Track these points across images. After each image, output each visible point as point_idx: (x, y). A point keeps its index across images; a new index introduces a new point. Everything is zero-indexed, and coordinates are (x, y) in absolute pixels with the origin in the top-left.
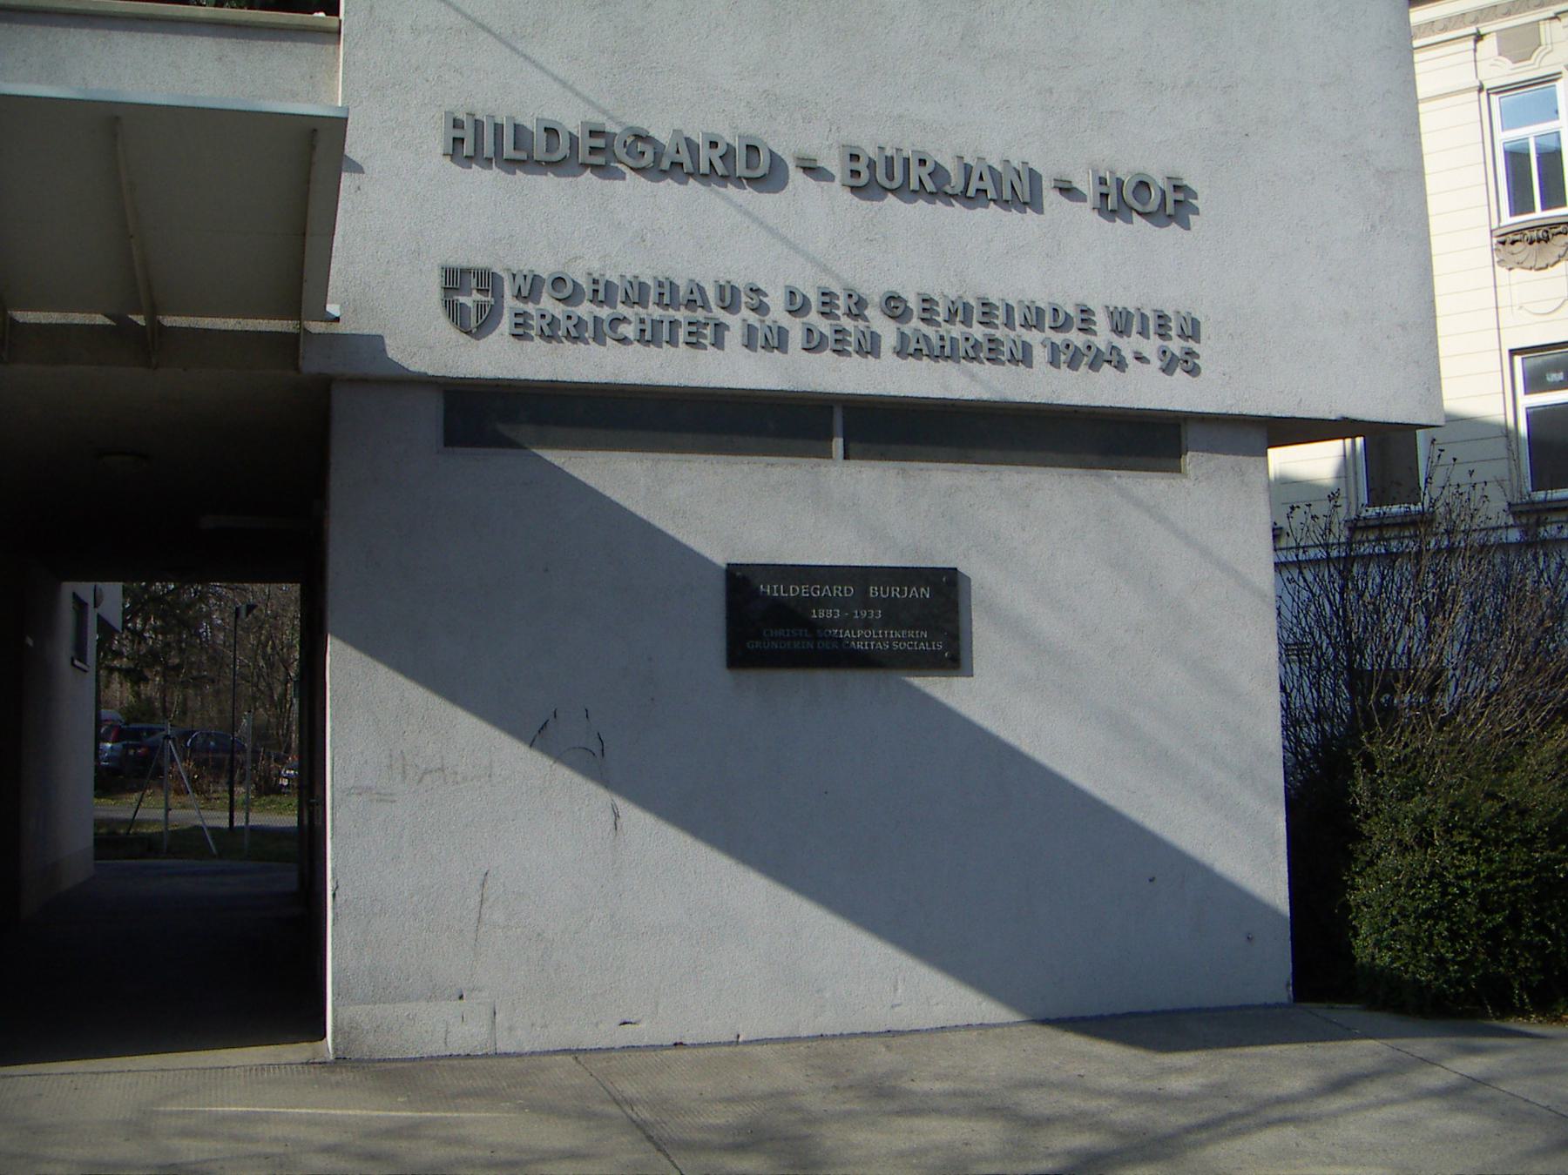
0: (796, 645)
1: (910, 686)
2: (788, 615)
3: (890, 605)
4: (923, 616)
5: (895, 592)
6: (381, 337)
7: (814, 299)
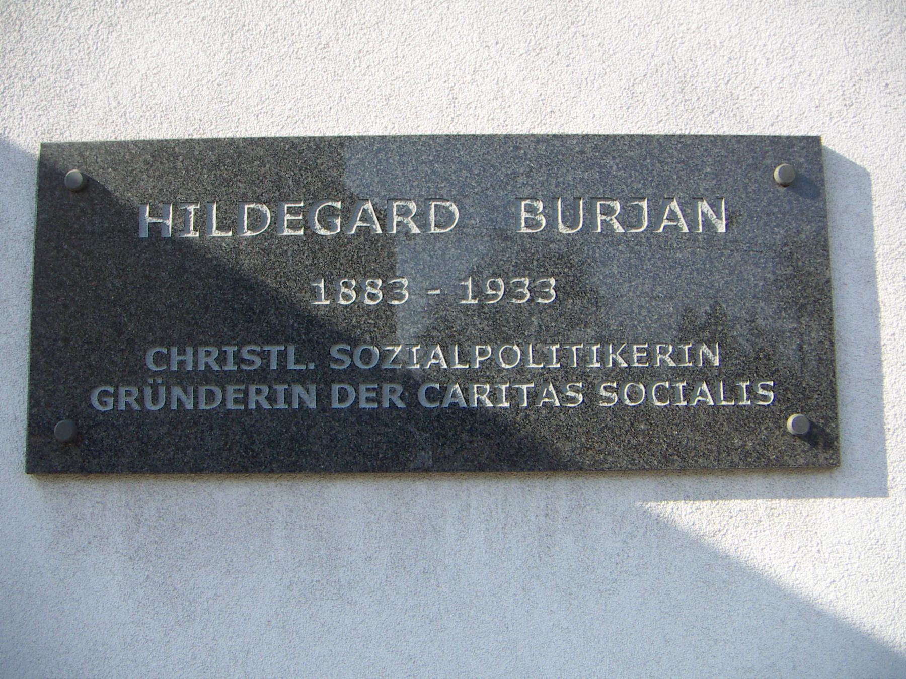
0: (257, 398)
1: (664, 528)
2: (241, 302)
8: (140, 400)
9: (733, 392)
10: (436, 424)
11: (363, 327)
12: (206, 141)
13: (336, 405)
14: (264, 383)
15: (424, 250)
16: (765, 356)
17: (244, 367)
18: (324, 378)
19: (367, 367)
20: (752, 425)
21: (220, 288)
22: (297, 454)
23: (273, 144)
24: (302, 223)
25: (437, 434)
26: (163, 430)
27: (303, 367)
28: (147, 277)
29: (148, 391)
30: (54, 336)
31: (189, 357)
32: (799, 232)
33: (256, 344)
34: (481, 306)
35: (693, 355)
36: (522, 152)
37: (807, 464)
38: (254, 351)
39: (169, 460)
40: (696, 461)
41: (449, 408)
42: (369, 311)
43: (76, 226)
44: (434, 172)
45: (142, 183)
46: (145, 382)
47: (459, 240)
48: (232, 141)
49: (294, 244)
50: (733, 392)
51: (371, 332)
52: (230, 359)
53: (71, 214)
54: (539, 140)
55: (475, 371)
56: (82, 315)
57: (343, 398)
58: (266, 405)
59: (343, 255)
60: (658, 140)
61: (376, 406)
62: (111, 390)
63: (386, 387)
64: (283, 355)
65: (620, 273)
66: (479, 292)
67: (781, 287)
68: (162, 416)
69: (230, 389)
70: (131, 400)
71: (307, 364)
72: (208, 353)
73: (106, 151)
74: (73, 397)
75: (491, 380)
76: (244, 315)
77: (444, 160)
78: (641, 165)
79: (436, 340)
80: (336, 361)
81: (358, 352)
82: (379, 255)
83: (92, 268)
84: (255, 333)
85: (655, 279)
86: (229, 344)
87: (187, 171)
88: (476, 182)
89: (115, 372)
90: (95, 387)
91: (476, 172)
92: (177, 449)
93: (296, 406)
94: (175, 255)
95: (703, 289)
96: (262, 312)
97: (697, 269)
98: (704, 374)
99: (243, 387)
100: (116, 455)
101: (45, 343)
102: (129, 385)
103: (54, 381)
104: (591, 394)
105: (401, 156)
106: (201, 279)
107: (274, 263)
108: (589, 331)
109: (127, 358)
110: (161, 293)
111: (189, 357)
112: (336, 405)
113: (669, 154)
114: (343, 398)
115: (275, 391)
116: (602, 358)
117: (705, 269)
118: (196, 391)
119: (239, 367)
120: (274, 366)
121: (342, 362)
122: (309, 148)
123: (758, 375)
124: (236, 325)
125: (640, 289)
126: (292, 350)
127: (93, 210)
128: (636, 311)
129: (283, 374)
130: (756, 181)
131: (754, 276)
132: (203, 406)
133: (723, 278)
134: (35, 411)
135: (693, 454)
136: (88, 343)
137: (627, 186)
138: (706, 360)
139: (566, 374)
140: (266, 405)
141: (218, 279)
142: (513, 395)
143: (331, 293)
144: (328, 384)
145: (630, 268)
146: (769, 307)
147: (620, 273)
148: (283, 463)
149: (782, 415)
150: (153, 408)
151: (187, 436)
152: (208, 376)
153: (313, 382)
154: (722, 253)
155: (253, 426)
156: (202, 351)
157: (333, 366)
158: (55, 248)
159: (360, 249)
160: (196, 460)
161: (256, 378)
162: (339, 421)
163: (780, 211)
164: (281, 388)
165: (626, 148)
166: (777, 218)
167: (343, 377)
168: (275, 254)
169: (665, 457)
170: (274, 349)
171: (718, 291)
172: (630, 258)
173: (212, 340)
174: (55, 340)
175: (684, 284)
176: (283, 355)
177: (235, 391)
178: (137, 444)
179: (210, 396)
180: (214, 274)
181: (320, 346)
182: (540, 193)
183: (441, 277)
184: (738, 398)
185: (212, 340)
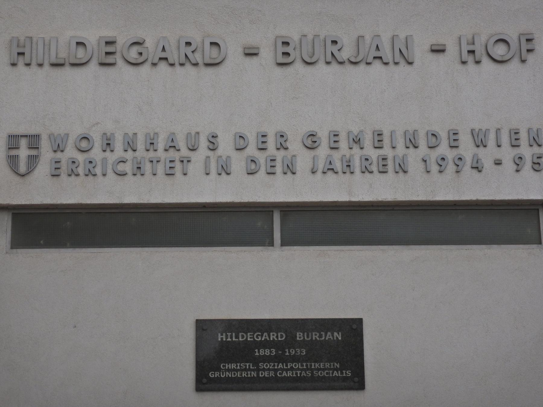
3: (310, 345)
4: (335, 351)
5: (315, 336)
7: (443, 135)
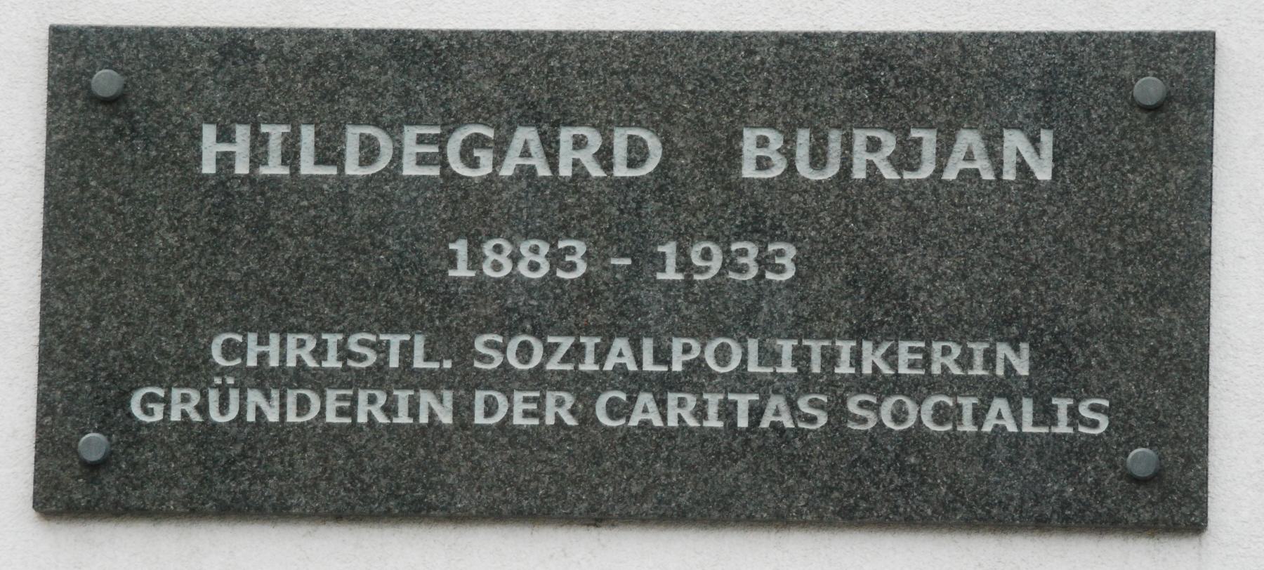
0: (369, 409)
2: (371, 261)
5: (870, 154)
6: (1214, 34)
8: (203, 409)
9: (1046, 414)
10: (620, 449)
11: (522, 309)
12: (300, 32)
13: (479, 419)
14: (380, 388)
15: (611, 202)
16: (1099, 364)
17: (351, 363)
18: (465, 381)
19: (526, 367)
20: (1074, 462)
21: (321, 250)
22: (424, 486)
23: (398, 40)
24: (439, 158)
25: (621, 463)
26: (236, 450)
27: (435, 365)
28: (214, 231)
29: (213, 395)
30: (77, 313)
31: (273, 348)
32: (1165, 180)
33: (370, 331)
34: (689, 282)
35: (990, 358)
36: (758, 58)
37: (1155, 522)
38: (367, 341)
39: (243, 492)
40: (989, 512)
41: (639, 427)
42: (526, 283)
43: (108, 153)
44: (628, 87)
45: (206, 92)
46: (209, 383)
47: (662, 189)
48: (337, 35)
49: (427, 189)
50: (1046, 414)
51: (533, 318)
52: (332, 352)
53: (100, 135)
54: (782, 40)
55: (677, 375)
56: (119, 285)
57: (490, 410)
58: (381, 419)
59: (496, 206)
60: (960, 40)
61: (536, 422)
62: (160, 392)
63: (551, 397)
64: (407, 349)
65: (892, 239)
66: (685, 265)
67: (1131, 261)
68: (235, 429)
69: (331, 395)
70: (189, 408)
71: (441, 362)
72: (301, 344)
73: (153, 43)
74: (105, 402)
75: (698, 390)
76: (354, 290)
77: (644, 69)
78: (932, 78)
79: (624, 330)
80: (482, 358)
81: (513, 345)
82: (547, 207)
83: (133, 215)
84: (368, 315)
85: (941, 248)
86: (330, 331)
87: (273, 76)
88: (689, 103)
89: (167, 367)
90: (137, 388)
91: (690, 88)
92: (255, 477)
93: (424, 419)
94: (254, 200)
95: (1013, 263)
96: (379, 286)
97: (1005, 235)
98: (1008, 388)
99: (350, 392)
100: (166, 484)
101: (64, 324)
102: (187, 386)
103: (76, 379)
104: (837, 412)
105: (582, 62)
106: (291, 235)
107: (397, 216)
108: (841, 321)
109: (185, 347)
110: (234, 255)
111: (273, 348)
112: (479, 419)
113: (974, 61)
114: (490, 410)
115: (395, 400)
116: (857, 359)
117: (1017, 235)
118: (283, 397)
119: (345, 364)
120: (394, 362)
121: (491, 359)
122: (450, 47)
123: (1086, 391)
124: (341, 304)
125: (919, 262)
126: (419, 342)
127: (133, 130)
128: (911, 294)
129: (408, 377)
130: (1106, 103)
131: (1092, 245)
132: (292, 417)
133: (1043, 248)
134: (48, 420)
135: (983, 502)
136: (128, 325)
137: (909, 111)
138: (1009, 368)
139: (805, 381)
140: (381, 419)
141: (317, 237)
142: (728, 411)
143: (475, 260)
144: (471, 391)
145: (906, 232)
146: (1110, 292)
147: (892, 239)
148: (404, 499)
149: (1121, 450)
150: (814, 176)
151: (270, 459)
152: (300, 376)
153: (449, 388)
154: (1044, 212)
155: (364, 447)
156: (292, 339)
157: (477, 365)
158: (77, 185)
159: (520, 198)
160: (281, 494)
161: (370, 380)
162: (483, 443)
163: (1138, 147)
164: (403, 396)
165: (910, 53)
166: (1132, 158)
167: (492, 380)
168: (399, 202)
169: (943, 504)
170: (395, 340)
171: (1034, 267)
172: (907, 217)
173: (308, 324)
174: (78, 319)
175: (984, 256)
176: (407, 349)
177: (339, 398)
178: (197, 470)
179: (303, 405)
180: (311, 230)
181: (461, 336)
182: (780, 120)
183: (634, 242)
184: (1054, 422)
185: (308, 324)
